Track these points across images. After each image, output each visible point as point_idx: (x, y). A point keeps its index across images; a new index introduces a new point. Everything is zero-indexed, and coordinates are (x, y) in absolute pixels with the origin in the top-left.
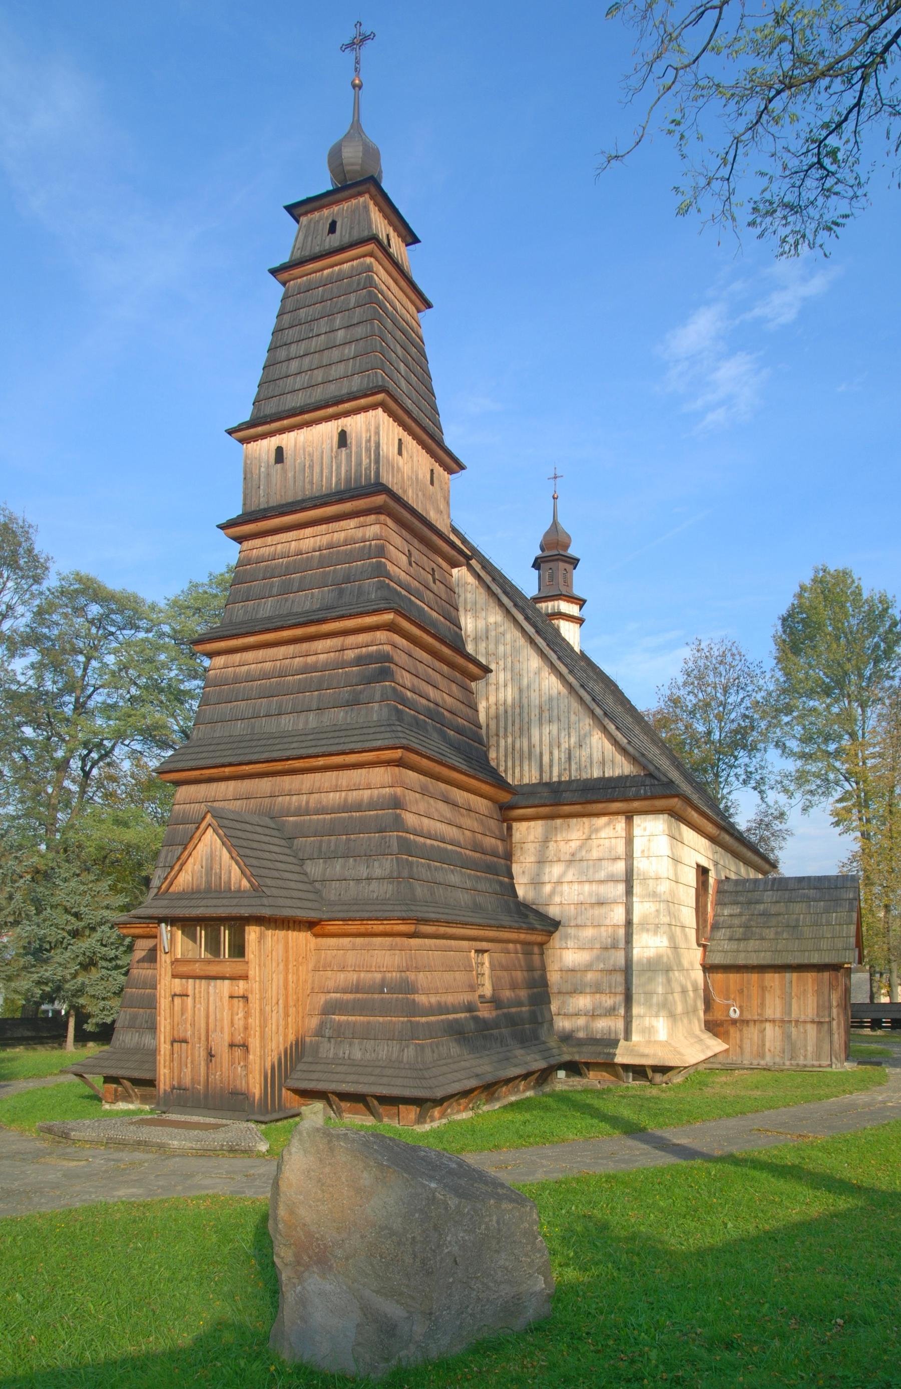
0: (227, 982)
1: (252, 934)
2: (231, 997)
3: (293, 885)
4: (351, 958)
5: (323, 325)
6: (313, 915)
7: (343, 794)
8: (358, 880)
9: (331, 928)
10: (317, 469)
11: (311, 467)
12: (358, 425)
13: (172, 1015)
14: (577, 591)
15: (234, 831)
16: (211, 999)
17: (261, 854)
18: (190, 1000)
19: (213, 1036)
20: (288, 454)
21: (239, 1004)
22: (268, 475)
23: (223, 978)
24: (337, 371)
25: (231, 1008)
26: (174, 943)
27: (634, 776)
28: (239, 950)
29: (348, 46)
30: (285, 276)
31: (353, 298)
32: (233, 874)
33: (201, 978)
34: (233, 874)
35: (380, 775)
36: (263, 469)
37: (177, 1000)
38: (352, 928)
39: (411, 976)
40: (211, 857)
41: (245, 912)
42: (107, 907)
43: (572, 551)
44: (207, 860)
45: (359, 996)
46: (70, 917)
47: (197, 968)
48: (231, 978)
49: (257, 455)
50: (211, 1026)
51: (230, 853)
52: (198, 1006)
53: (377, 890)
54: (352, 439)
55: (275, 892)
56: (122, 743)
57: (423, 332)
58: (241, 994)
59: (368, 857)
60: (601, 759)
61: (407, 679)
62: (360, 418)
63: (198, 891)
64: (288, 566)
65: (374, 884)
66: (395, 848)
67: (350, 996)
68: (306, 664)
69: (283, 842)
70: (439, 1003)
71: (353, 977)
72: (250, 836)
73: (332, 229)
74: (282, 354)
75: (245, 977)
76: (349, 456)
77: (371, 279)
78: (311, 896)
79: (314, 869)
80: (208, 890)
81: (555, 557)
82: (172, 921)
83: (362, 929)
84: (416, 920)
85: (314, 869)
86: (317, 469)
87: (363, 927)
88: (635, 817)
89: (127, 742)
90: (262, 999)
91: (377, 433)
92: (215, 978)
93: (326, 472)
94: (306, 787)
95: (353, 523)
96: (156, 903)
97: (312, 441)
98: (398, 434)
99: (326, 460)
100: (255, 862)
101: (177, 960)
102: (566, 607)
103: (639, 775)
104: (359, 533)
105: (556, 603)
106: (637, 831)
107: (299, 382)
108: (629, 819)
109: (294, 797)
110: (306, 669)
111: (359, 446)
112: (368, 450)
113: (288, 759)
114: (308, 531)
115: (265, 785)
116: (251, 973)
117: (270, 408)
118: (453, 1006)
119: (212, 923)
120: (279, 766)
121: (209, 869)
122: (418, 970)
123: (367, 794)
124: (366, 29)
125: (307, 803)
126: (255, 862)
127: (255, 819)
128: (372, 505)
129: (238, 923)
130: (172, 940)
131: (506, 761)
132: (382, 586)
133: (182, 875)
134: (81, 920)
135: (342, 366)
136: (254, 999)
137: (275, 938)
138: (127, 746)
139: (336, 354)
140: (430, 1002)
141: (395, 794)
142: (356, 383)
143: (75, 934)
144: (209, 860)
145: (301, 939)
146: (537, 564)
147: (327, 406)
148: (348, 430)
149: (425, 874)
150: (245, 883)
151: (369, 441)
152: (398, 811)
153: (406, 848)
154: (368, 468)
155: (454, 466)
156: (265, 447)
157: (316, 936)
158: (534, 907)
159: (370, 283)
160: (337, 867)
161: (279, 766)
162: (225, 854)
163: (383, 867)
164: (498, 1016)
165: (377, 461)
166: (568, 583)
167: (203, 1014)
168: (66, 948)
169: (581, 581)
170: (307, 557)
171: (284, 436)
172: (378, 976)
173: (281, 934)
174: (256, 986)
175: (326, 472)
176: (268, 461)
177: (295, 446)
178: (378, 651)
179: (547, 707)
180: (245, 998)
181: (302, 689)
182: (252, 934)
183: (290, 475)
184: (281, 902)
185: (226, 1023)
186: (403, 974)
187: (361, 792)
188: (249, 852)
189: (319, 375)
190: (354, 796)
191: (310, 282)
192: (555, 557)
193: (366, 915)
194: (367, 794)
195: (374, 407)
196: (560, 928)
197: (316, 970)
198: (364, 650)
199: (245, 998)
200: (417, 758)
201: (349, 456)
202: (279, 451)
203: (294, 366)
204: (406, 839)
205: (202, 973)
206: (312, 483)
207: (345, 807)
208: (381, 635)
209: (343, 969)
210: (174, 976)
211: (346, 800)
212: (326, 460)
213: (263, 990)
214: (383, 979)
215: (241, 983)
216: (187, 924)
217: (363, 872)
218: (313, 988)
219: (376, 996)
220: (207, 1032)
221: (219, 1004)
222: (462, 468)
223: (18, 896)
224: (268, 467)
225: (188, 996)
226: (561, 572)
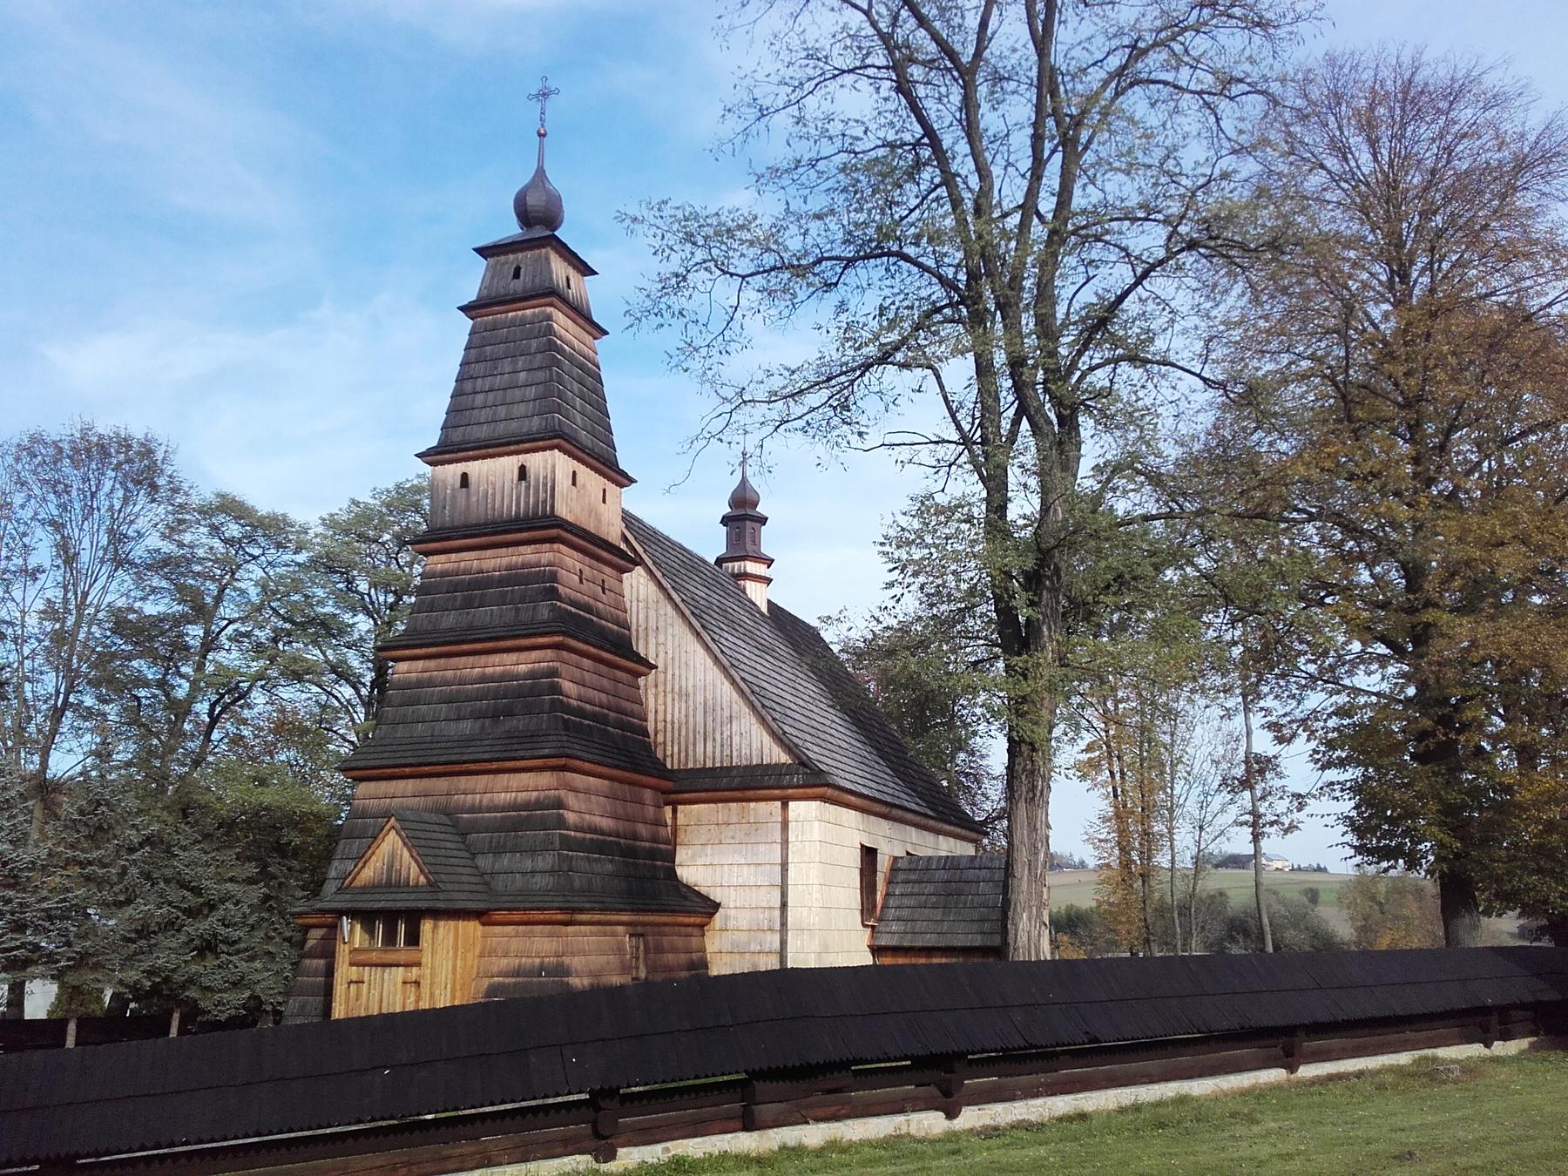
1: (427, 926)
2: (405, 983)
3: (464, 878)
4: (515, 944)
5: (506, 365)
6: (482, 906)
8: (524, 873)
9: (497, 917)
11: (494, 495)
12: (537, 462)
13: (347, 1002)
14: (766, 550)
15: (415, 832)
17: (437, 852)
20: (472, 479)
21: (412, 989)
22: (454, 497)
23: (398, 965)
24: (520, 409)
25: (404, 993)
26: (353, 934)
28: (413, 939)
29: (537, 96)
30: (473, 313)
31: (534, 344)
32: (411, 870)
33: (376, 965)
34: (411, 870)
35: (546, 779)
37: (353, 987)
38: (516, 917)
39: (566, 960)
40: (393, 856)
41: (422, 905)
42: (232, 880)
46: (187, 893)
47: (374, 957)
48: (406, 965)
53: (540, 882)
55: (449, 887)
57: (600, 359)
59: (533, 852)
62: (538, 456)
63: (380, 886)
64: (470, 582)
65: (538, 877)
66: (557, 844)
67: (507, 980)
69: (457, 838)
72: (428, 835)
73: (517, 275)
74: (468, 386)
75: (419, 964)
77: (550, 328)
78: (478, 888)
79: (484, 862)
80: (389, 884)
81: (743, 517)
82: (354, 914)
83: (525, 918)
84: (565, 907)
85: (484, 862)
90: (432, 984)
91: (553, 472)
92: (391, 965)
94: (480, 787)
96: (339, 897)
97: (494, 474)
100: (432, 860)
101: (355, 950)
102: (752, 567)
104: (533, 558)
107: (484, 415)
108: (785, 806)
110: (483, 679)
111: (537, 481)
113: (465, 762)
114: (489, 553)
115: (442, 784)
116: (424, 960)
117: (457, 435)
119: (390, 917)
120: (457, 768)
122: (573, 954)
124: (552, 85)
126: (432, 860)
127: (433, 817)
129: (414, 918)
130: (352, 931)
132: (553, 608)
133: (366, 870)
134: (201, 895)
135: (522, 407)
136: (425, 983)
137: (446, 928)
139: (518, 393)
142: (536, 423)
143: (191, 913)
144: (390, 856)
145: (472, 928)
146: (725, 521)
147: (508, 444)
148: (527, 465)
149: (583, 865)
150: (422, 879)
154: (545, 501)
156: (452, 472)
157: (484, 924)
159: (550, 331)
160: (506, 861)
161: (457, 768)
162: (406, 854)
163: (546, 861)
165: (553, 496)
166: (756, 541)
167: (377, 998)
168: (178, 931)
169: (768, 541)
172: (537, 961)
173: (452, 923)
174: (428, 971)
180: (417, 983)
181: (480, 697)
182: (427, 926)
183: (474, 499)
184: (455, 896)
188: (427, 851)
189: (502, 411)
191: (495, 321)
193: (528, 905)
195: (551, 448)
197: (481, 956)
199: (417, 983)
200: (578, 763)
201: (528, 488)
202: (465, 477)
203: (479, 399)
207: (514, 806)
210: (351, 965)
213: (433, 975)
216: (366, 918)
217: (528, 865)
222: (632, 481)
223: (134, 871)
224: (453, 489)
226: (749, 531)
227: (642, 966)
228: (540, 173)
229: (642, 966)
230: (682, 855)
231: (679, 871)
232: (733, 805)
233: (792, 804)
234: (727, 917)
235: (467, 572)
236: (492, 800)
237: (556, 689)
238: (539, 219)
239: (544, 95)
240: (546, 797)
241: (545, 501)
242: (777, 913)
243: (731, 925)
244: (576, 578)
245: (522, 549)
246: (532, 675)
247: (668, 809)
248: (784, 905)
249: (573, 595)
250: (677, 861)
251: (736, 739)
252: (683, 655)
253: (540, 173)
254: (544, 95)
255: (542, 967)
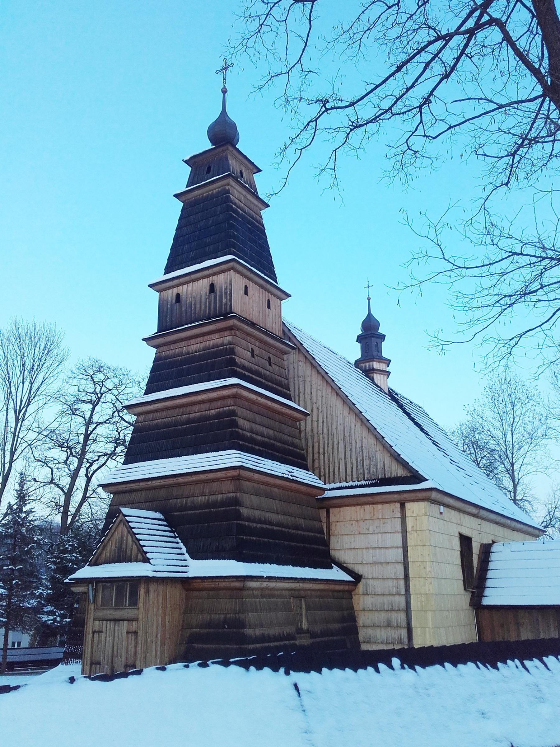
0: (126, 622)
2: (128, 633)
7: (207, 497)
10: (198, 306)
11: (195, 304)
16: (116, 634)
18: (104, 634)
19: (115, 660)
20: (183, 297)
21: (132, 637)
22: (172, 310)
23: (124, 620)
25: (127, 638)
27: (404, 477)
28: (134, 602)
29: (221, 71)
31: (219, 209)
33: (110, 620)
36: (169, 306)
39: (242, 616)
43: (381, 331)
44: (119, 542)
45: (211, 630)
48: (128, 620)
49: (166, 298)
50: (115, 653)
51: (132, 538)
52: (108, 639)
54: (217, 289)
56: (111, 458)
58: (134, 630)
60: (382, 467)
61: (246, 424)
68: (189, 418)
70: (263, 635)
71: (207, 617)
75: (137, 620)
76: (215, 297)
86: (198, 306)
87: (213, 583)
88: (406, 504)
89: (114, 458)
91: (231, 284)
93: (203, 307)
95: (217, 336)
98: (245, 283)
99: (203, 300)
102: (376, 365)
103: (407, 476)
104: (220, 341)
105: (371, 363)
106: (408, 513)
108: (403, 506)
109: (179, 500)
111: (221, 292)
112: (226, 293)
116: (140, 616)
118: (274, 636)
121: (120, 548)
123: (220, 497)
125: (186, 503)
128: (227, 325)
131: (324, 469)
138: (114, 460)
140: (255, 634)
141: (236, 497)
148: (215, 283)
151: (226, 289)
152: (238, 507)
153: (242, 530)
154: (226, 304)
155: (283, 296)
158: (345, 565)
164: (312, 644)
165: (231, 300)
166: (379, 349)
169: (386, 350)
170: (192, 356)
171: (181, 287)
172: (222, 616)
175: (203, 307)
176: (172, 302)
177: (187, 293)
178: (229, 410)
179: (348, 435)
185: (124, 651)
186: (237, 615)
187: (217, 496)
190: (213, 498)
192: (371, 336)
194: (220, 497)
196: (362, 580)
198: (221, 409)
199: (136, 633)
201: (215, 297)
202: (178, 296)
204: (241, 525)
205: (111, 617)
206: (195, 313)
207: (208, 505)
208: (230, 401)
209: (202, 612)
211: (208, 500)
212: (203, 300)
214: (225, 618)
215: (134, 623)
218: (183, 625)
219: (220, 631)
220: (112, 656)
221: (120, 637)
222: (289, 296)
224: (172, 305)
225: (102, 632)
227: (304, 620)
228: (224, 112)
229: (304, 620)
230: (334, 543)
231: (332, 553)
232: (367, 507)
233: (408, 505)
234: (367, 585)
235: (180, 355)
236: (193, 502)
237: (234, 424)
238: (223, 134)
239: (225, 69)
240: (227, 498)
241: (226, 304)
242: (402, 582)
243: (370, 590)
244: (249, 354)
245: (212, 336)
246: (218, 416)
247: (323, 513)
248: (406, 577)
249: (246, 364)
250: (332, 546)
251: (366, 462)
252: (329, 408)
253: (224, 112)
254: (225, 69)
255: (225, 621)
